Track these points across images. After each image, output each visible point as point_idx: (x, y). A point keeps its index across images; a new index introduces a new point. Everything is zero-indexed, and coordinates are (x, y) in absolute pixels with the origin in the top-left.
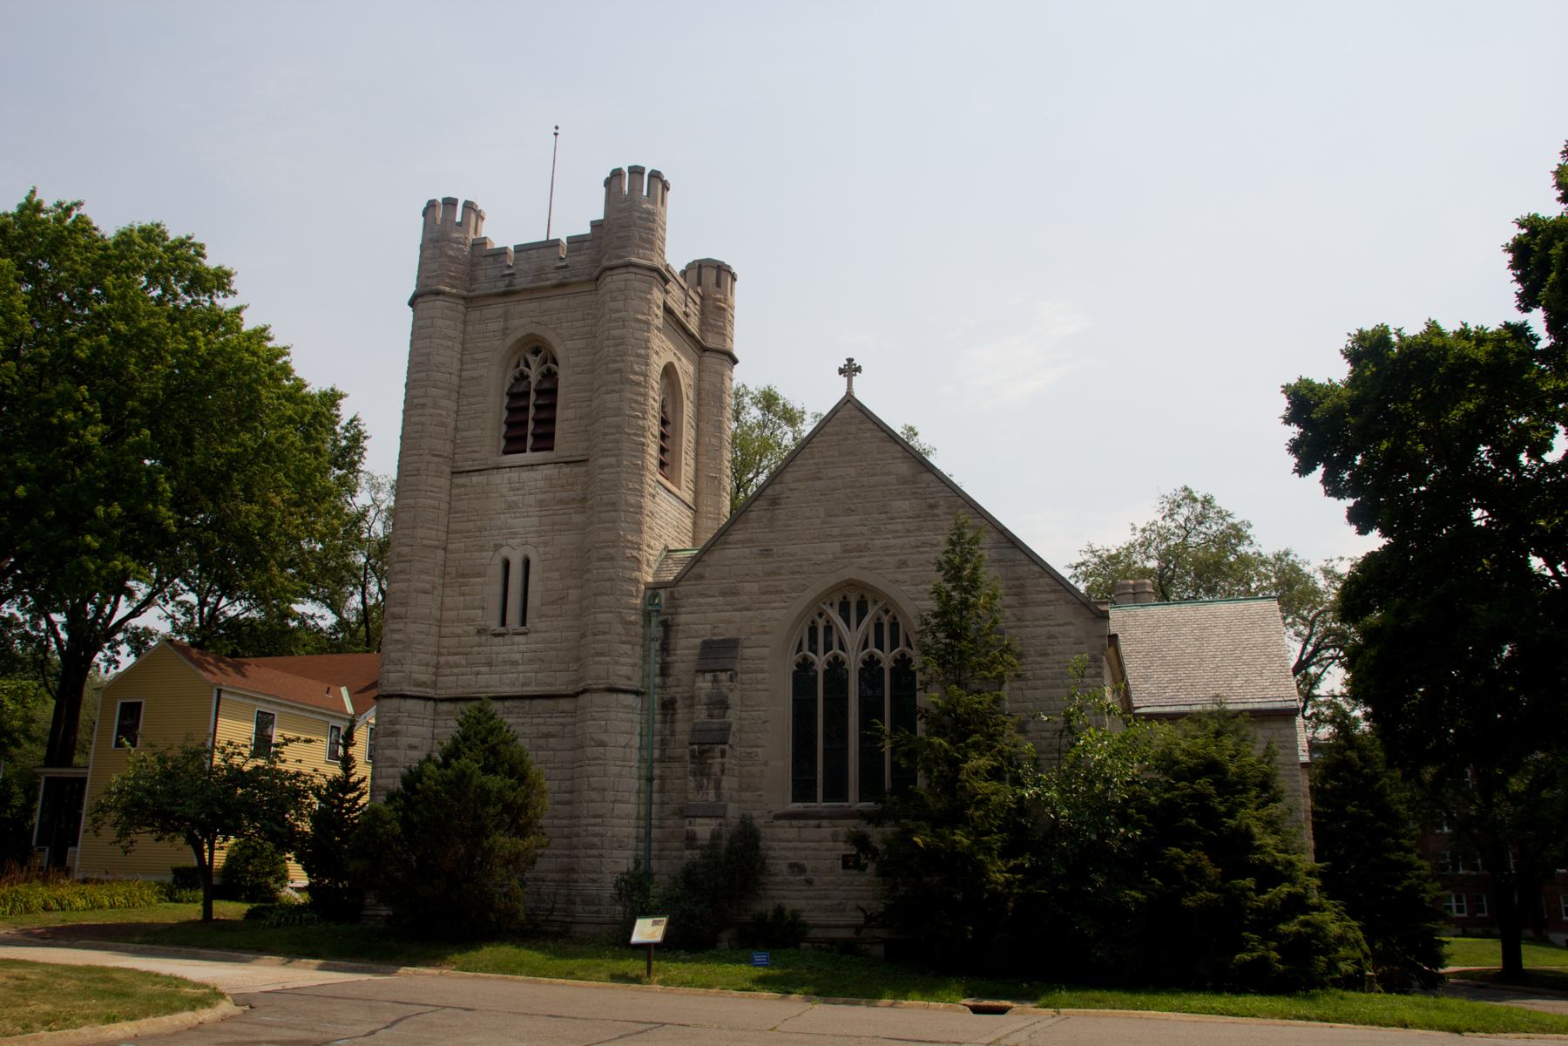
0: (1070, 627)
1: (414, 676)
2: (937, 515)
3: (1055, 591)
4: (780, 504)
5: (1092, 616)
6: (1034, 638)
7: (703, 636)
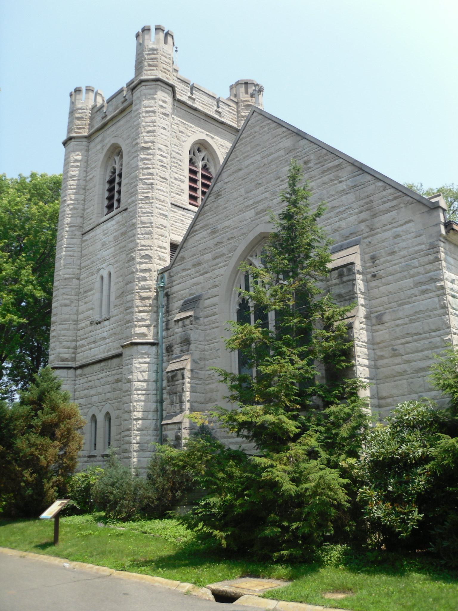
0: (411, 224)
1: (61, 355)
2: (310, 168)
3: (395, 198)
4: (221, 195)
5: (426, 209)
6: (383, 241)
7: (185, 297)
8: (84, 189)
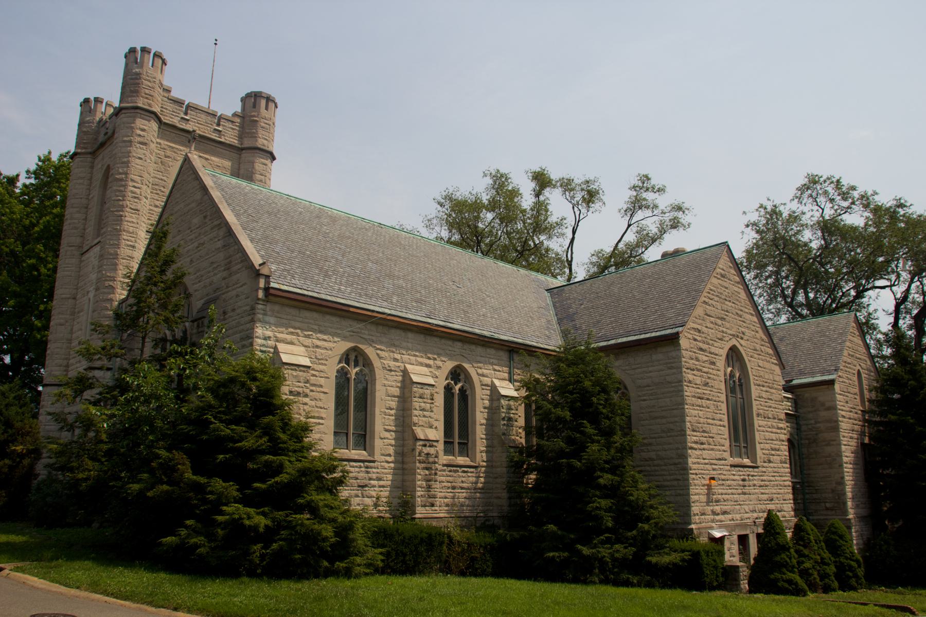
8: (87, 208)
